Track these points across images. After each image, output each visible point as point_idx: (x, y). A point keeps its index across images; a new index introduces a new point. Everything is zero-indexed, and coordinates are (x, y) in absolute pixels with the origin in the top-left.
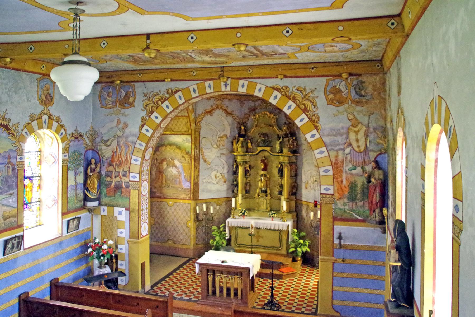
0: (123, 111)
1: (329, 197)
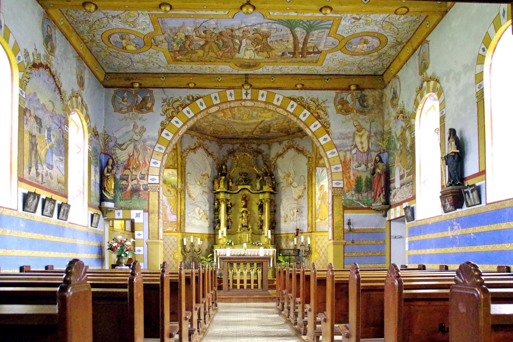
0: (140, 115)
1: (340, 190)
